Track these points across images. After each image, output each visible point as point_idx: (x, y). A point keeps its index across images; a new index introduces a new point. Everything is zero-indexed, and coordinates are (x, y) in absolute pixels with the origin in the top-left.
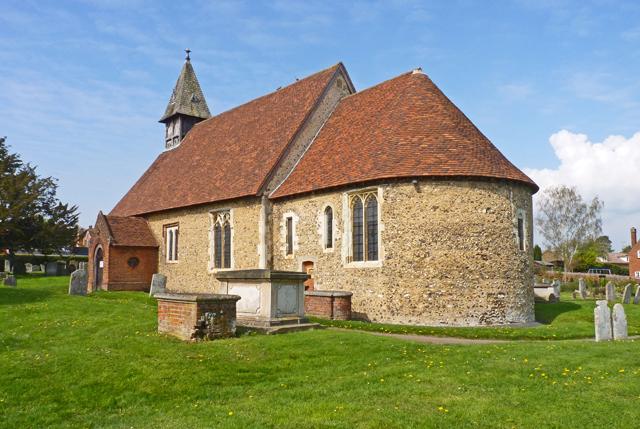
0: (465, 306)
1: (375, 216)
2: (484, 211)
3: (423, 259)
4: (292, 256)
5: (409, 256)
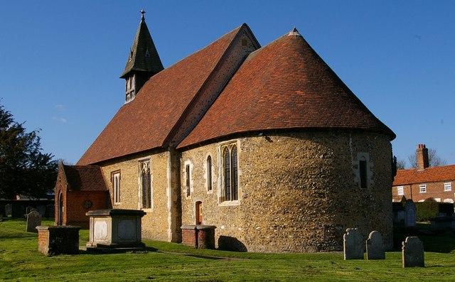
4: (190, 197)
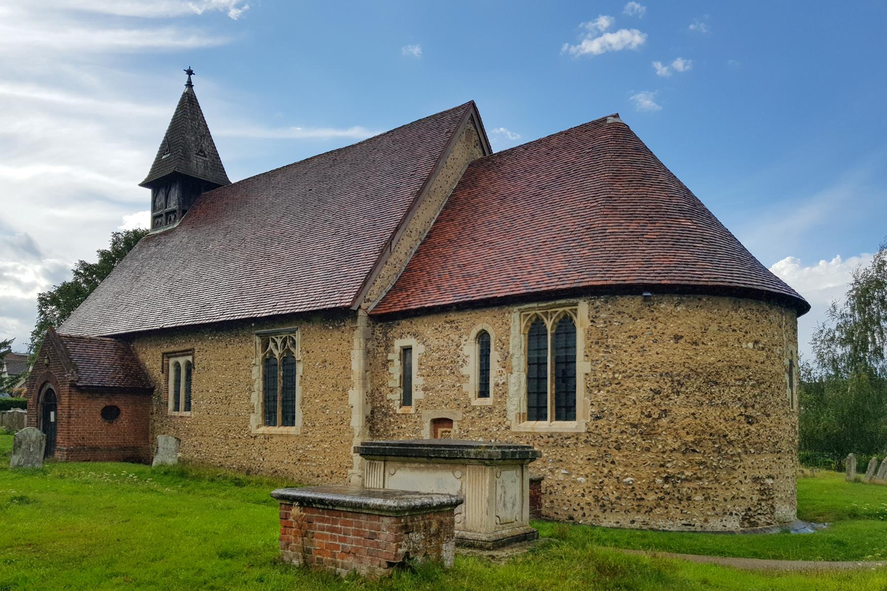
0: (720, 499)
2: (751, 345)
3: (657, 419)
4: (412, 410)
5: (633, 415)
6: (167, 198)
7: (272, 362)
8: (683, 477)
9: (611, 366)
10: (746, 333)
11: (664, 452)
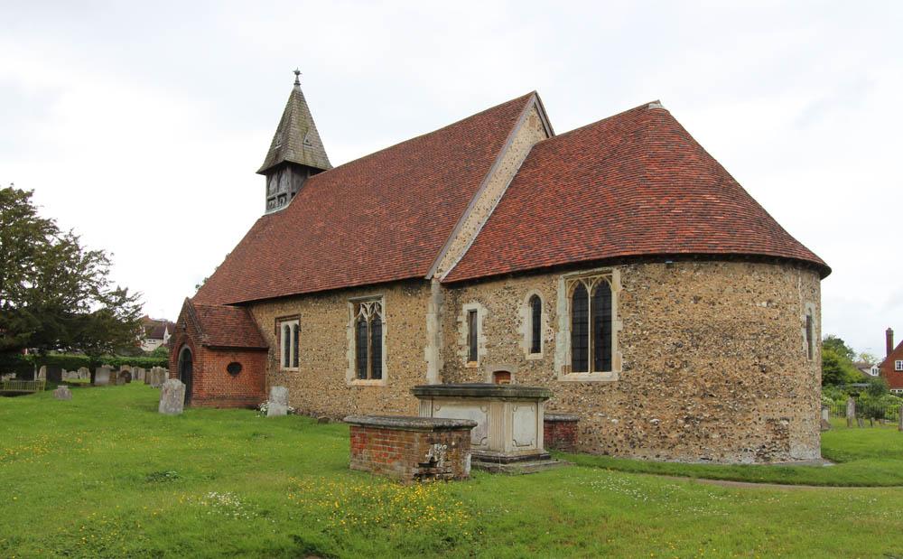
1: (607, 308)
2: (764, 304)
3: (678, 369)
4: (477, 364)
5: (658, 365)
6: (279, 182)
7: (363, 324)
8: (702, 418)
9: (640, 324)
10: (760, 293)
11: (685, 397)
